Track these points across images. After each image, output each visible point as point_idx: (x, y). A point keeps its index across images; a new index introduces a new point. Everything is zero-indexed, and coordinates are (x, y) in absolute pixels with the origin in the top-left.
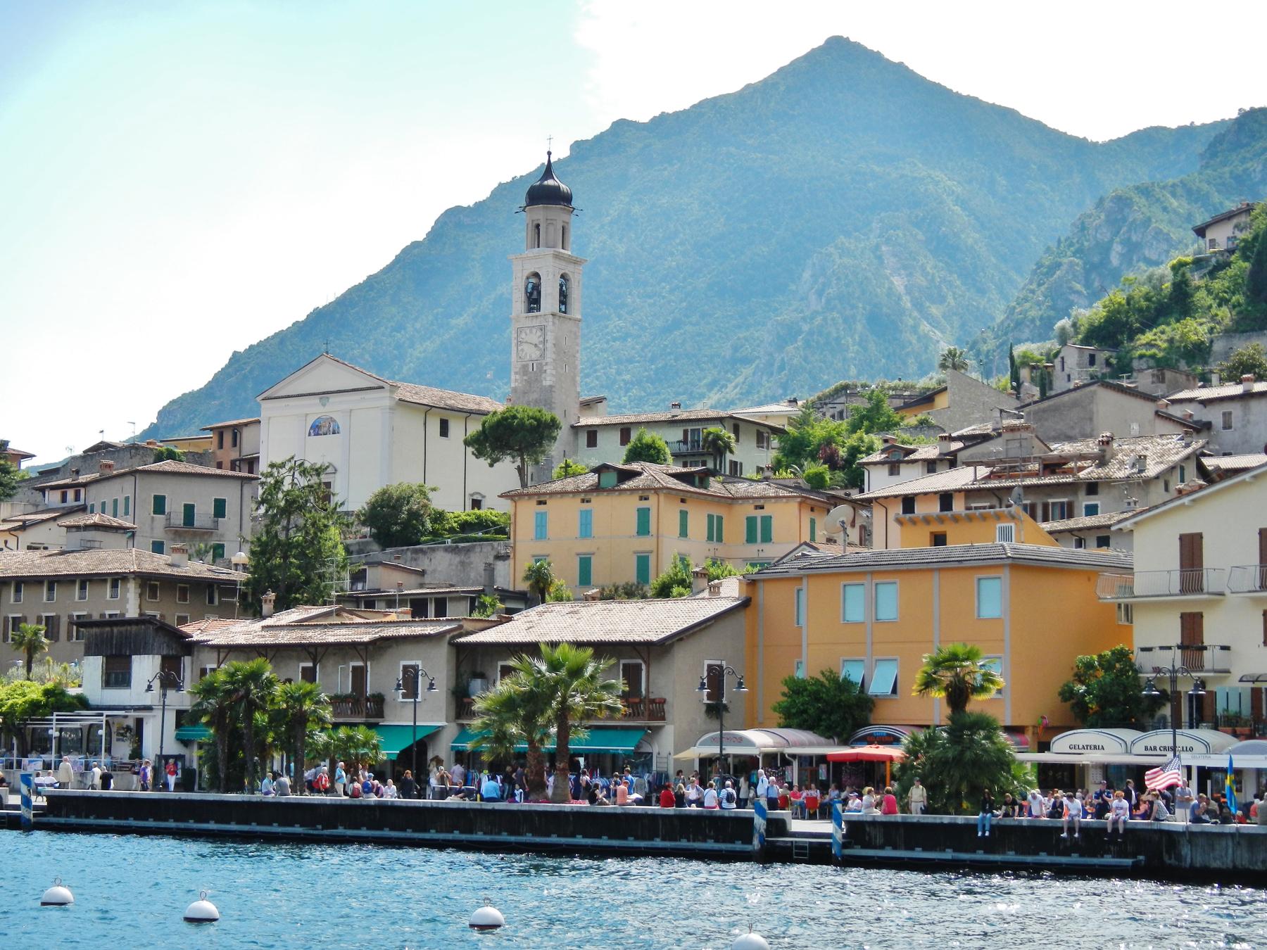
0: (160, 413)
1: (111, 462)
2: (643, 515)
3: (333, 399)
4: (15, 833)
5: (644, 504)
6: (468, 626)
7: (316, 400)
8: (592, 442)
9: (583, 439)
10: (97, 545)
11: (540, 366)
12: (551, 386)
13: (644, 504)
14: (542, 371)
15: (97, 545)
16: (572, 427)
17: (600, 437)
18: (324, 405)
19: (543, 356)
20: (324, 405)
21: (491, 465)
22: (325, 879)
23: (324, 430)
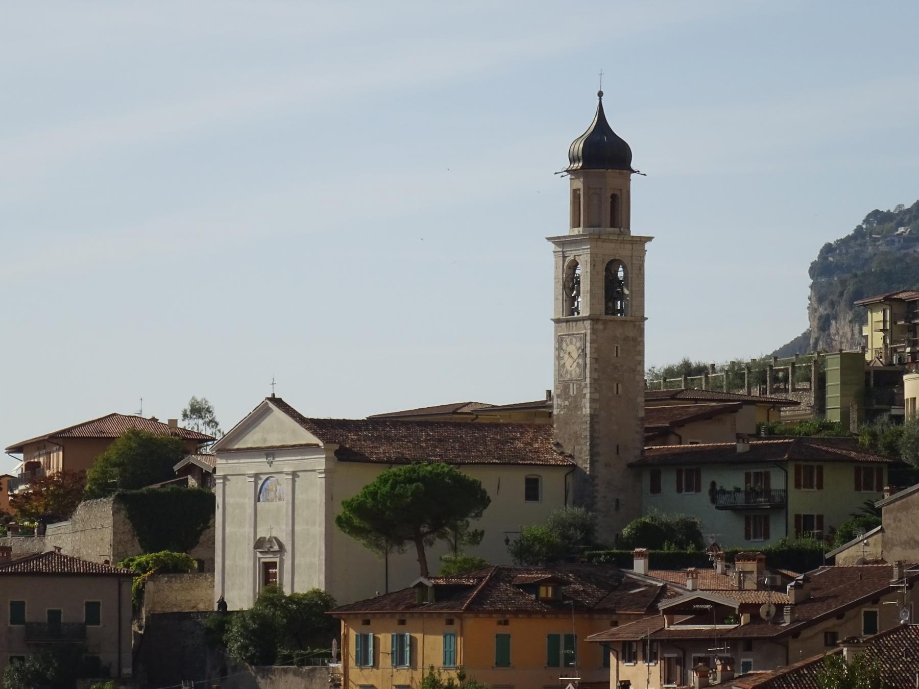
5: (503, 630)
13: (503, 630)
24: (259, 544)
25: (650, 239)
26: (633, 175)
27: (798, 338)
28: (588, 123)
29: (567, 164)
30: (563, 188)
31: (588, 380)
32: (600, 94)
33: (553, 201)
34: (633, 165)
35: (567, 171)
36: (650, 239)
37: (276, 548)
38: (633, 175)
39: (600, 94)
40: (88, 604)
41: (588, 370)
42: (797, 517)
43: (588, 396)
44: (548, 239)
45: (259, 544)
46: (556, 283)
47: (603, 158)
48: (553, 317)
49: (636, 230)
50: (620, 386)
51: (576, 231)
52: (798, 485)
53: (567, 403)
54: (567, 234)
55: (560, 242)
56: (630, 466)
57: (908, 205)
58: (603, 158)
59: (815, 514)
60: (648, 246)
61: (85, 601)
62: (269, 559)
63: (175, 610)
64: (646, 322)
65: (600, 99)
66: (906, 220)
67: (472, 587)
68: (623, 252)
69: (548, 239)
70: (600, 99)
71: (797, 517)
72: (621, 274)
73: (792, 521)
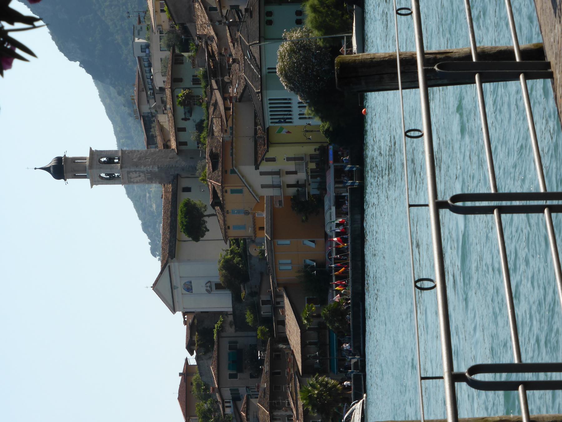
0: (71, 59)
1: (211, 388)
2: (233, 192)
3: (174, 283)
4: (366, 297)
5: (229, 191)
6: (296, 370)
7: (175, 292)
8: (185, 144)
9: (183, 147)
10: (255, 414)
11: (148, 173)
12: (158, 168)
13: (229, 191)
14: (151, 172)
15: (255, 414)
16: (178, 154)
17: (182, 140)
18: (177, 288)
19: (143, 172)
20: (177, 288)
21: (208, 230)
22: (386, 178)
23: (189, 287)
24: (209, 292)
25: (91, 148)
28: (48, 175)
30: (71, 182)
32: (35, 169)
33: (79, 186)
34: (62, 156)
36: (91, 148)
37: (208, 285)
39: (35, 169)
44: (92, 187)
45: (209, 292)
47: (61, 169)
57: (49, 31)
58: (61, 169)
59: (192, 78)
60: (93, 149)
62: (214, 287)
66: (403, 244)
67: (346, 272)
69: (92, 187)
71: (193, 84)
72: (105, 159)
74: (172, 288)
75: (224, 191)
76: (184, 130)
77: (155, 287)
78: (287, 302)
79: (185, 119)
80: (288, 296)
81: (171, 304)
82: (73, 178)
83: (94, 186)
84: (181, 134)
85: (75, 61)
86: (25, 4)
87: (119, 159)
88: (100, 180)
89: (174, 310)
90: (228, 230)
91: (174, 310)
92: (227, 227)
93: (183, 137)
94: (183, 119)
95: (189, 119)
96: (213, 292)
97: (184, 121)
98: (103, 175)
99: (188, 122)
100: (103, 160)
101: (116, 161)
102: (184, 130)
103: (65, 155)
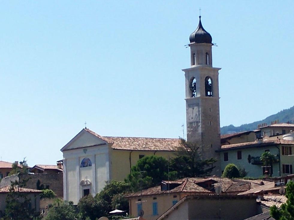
18: (85, 153)
23: (86, 164)
25: (220, 69)
26: (213, 46)
27: (226, 127)
28: (194, 30)
29: (189, 42)
31: (200, 120)
32: (200, 17)
33: (184, 59)
35: (189, 45)
36: (220, 69)
38: (213, 46)
39: (200, 17)
40: (227, 160)
41: (200, 116)
42: (283, 165)
43: (200, 126)
44: (183, 70)
45: (82, 184)
46: (186, 86)
47: (202, 41)
48: (185, 98)
49: (214, 65)
50: (212, 122)
51: (193, 66)
52: (283, 154)
53: (192, 129)
54: (190, 68)
55: (187, 71)
56: (216, 151)
58: (202, 41)
60: (219, 71)
61: (224, 161)
62: (86, 188)
63: (224, 138)
64: (220, 99)
65: (200, 19)
68: (211, 74)
69: (183, 70)
70: (200, 19)
71: (283, 165)
72: (210, 82)
73: (282, 166)
74: (85, 149)
75: (175, 195)
76: (240, 157)
77: (85, 132)
78: (121, 211)
79: (250, 158)
80: (123, 212)
81: (71, 148)
82: (192, 52)
83: (184, 73)
84: (235, 155)
85: (224, 127)
86: (263, 120)
87: (210, 96)
88: (190, 78)
89: (64, 150)
90: (137, 199)
91: (64, 150)
92: (140, 198)
93: (233, 156)
94: (249, 156)
95: (250, 162)
96: (81, 187)
97: (248, 157)
98: (195, 81)
99: (247, 161)
100: (209, 80)
101: (209, 93)
102: (240, 157)
103: (213, 44)
